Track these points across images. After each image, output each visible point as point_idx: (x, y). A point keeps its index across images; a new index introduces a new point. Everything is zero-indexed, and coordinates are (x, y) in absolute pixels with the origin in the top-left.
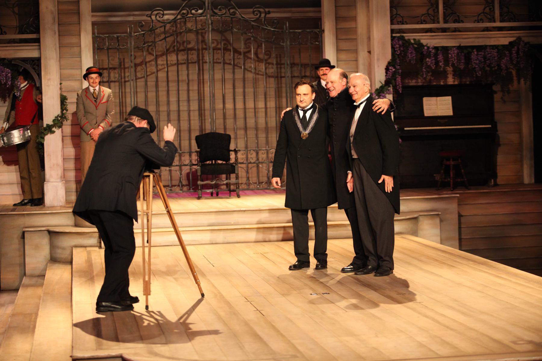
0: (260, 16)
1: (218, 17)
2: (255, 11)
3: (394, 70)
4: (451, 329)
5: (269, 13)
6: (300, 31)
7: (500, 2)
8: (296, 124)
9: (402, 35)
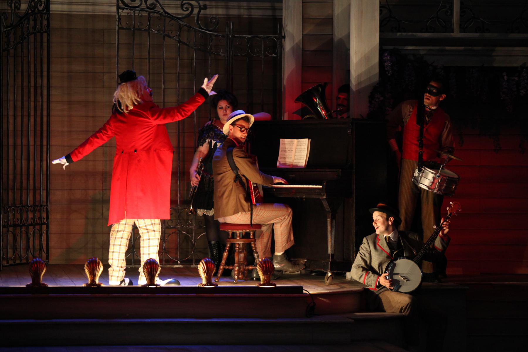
0: (192, 11)
1: (129, 11)
2: (185, 4)
3: (382, 98)
4: (14, 91)
5: (205, 7)
6: (249, 36)
7: (461, 3)
8: (327, 227)
9: (397, 47)
